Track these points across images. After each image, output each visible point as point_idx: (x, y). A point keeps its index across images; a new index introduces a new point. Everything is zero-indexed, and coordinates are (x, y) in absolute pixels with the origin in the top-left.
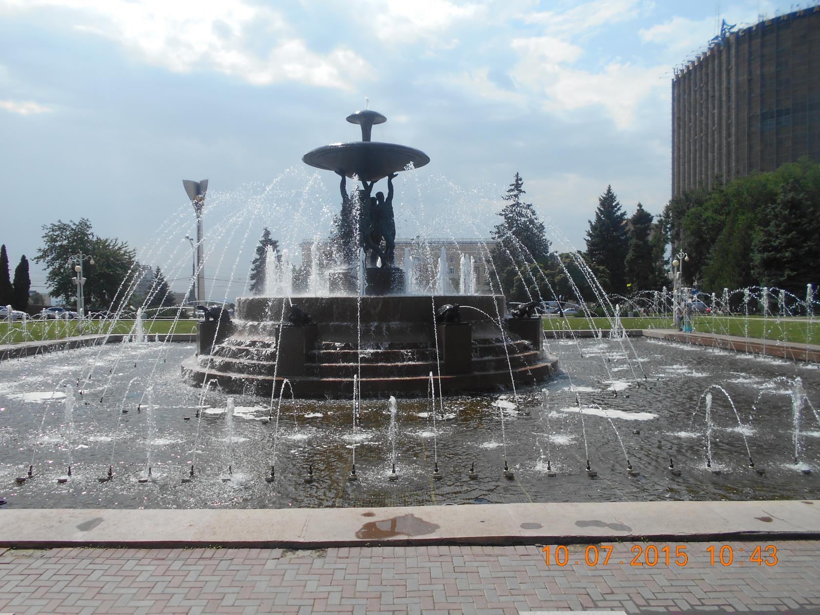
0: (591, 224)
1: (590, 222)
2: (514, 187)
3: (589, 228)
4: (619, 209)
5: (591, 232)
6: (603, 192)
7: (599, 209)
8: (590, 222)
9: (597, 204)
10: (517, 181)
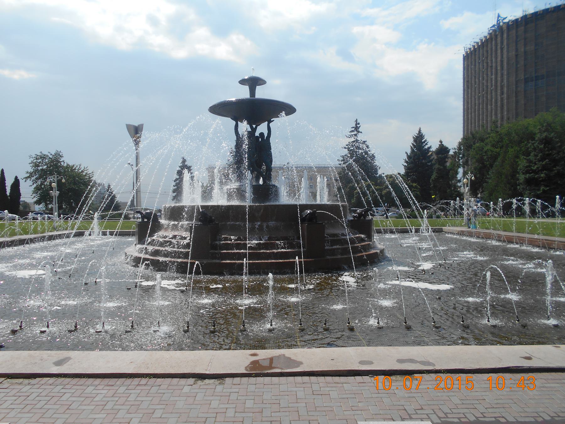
0: (407, 155)
1: (406, 153)
2: (354, 129)
3: (406, 157)
4: (426, 144)
5: (407, 160)
6: (415, 133)
7: (413, 144)
8: (406, 153)
9: (412, 140)
10: (356, 124)
